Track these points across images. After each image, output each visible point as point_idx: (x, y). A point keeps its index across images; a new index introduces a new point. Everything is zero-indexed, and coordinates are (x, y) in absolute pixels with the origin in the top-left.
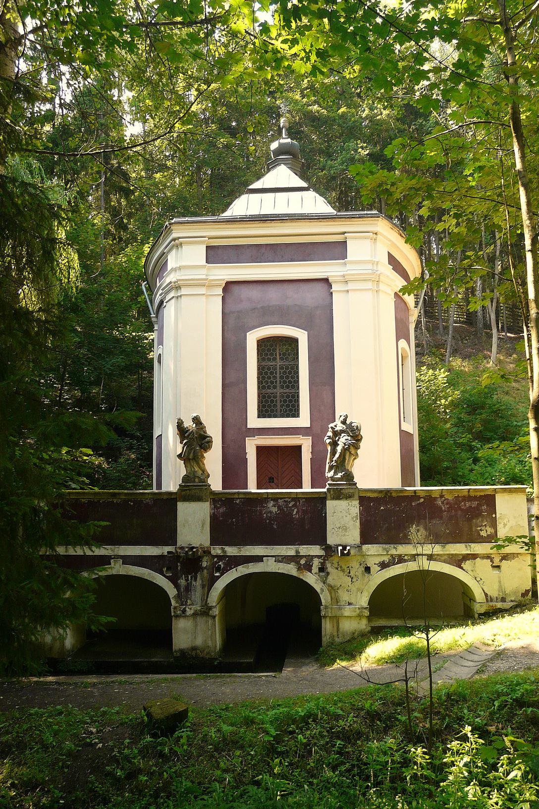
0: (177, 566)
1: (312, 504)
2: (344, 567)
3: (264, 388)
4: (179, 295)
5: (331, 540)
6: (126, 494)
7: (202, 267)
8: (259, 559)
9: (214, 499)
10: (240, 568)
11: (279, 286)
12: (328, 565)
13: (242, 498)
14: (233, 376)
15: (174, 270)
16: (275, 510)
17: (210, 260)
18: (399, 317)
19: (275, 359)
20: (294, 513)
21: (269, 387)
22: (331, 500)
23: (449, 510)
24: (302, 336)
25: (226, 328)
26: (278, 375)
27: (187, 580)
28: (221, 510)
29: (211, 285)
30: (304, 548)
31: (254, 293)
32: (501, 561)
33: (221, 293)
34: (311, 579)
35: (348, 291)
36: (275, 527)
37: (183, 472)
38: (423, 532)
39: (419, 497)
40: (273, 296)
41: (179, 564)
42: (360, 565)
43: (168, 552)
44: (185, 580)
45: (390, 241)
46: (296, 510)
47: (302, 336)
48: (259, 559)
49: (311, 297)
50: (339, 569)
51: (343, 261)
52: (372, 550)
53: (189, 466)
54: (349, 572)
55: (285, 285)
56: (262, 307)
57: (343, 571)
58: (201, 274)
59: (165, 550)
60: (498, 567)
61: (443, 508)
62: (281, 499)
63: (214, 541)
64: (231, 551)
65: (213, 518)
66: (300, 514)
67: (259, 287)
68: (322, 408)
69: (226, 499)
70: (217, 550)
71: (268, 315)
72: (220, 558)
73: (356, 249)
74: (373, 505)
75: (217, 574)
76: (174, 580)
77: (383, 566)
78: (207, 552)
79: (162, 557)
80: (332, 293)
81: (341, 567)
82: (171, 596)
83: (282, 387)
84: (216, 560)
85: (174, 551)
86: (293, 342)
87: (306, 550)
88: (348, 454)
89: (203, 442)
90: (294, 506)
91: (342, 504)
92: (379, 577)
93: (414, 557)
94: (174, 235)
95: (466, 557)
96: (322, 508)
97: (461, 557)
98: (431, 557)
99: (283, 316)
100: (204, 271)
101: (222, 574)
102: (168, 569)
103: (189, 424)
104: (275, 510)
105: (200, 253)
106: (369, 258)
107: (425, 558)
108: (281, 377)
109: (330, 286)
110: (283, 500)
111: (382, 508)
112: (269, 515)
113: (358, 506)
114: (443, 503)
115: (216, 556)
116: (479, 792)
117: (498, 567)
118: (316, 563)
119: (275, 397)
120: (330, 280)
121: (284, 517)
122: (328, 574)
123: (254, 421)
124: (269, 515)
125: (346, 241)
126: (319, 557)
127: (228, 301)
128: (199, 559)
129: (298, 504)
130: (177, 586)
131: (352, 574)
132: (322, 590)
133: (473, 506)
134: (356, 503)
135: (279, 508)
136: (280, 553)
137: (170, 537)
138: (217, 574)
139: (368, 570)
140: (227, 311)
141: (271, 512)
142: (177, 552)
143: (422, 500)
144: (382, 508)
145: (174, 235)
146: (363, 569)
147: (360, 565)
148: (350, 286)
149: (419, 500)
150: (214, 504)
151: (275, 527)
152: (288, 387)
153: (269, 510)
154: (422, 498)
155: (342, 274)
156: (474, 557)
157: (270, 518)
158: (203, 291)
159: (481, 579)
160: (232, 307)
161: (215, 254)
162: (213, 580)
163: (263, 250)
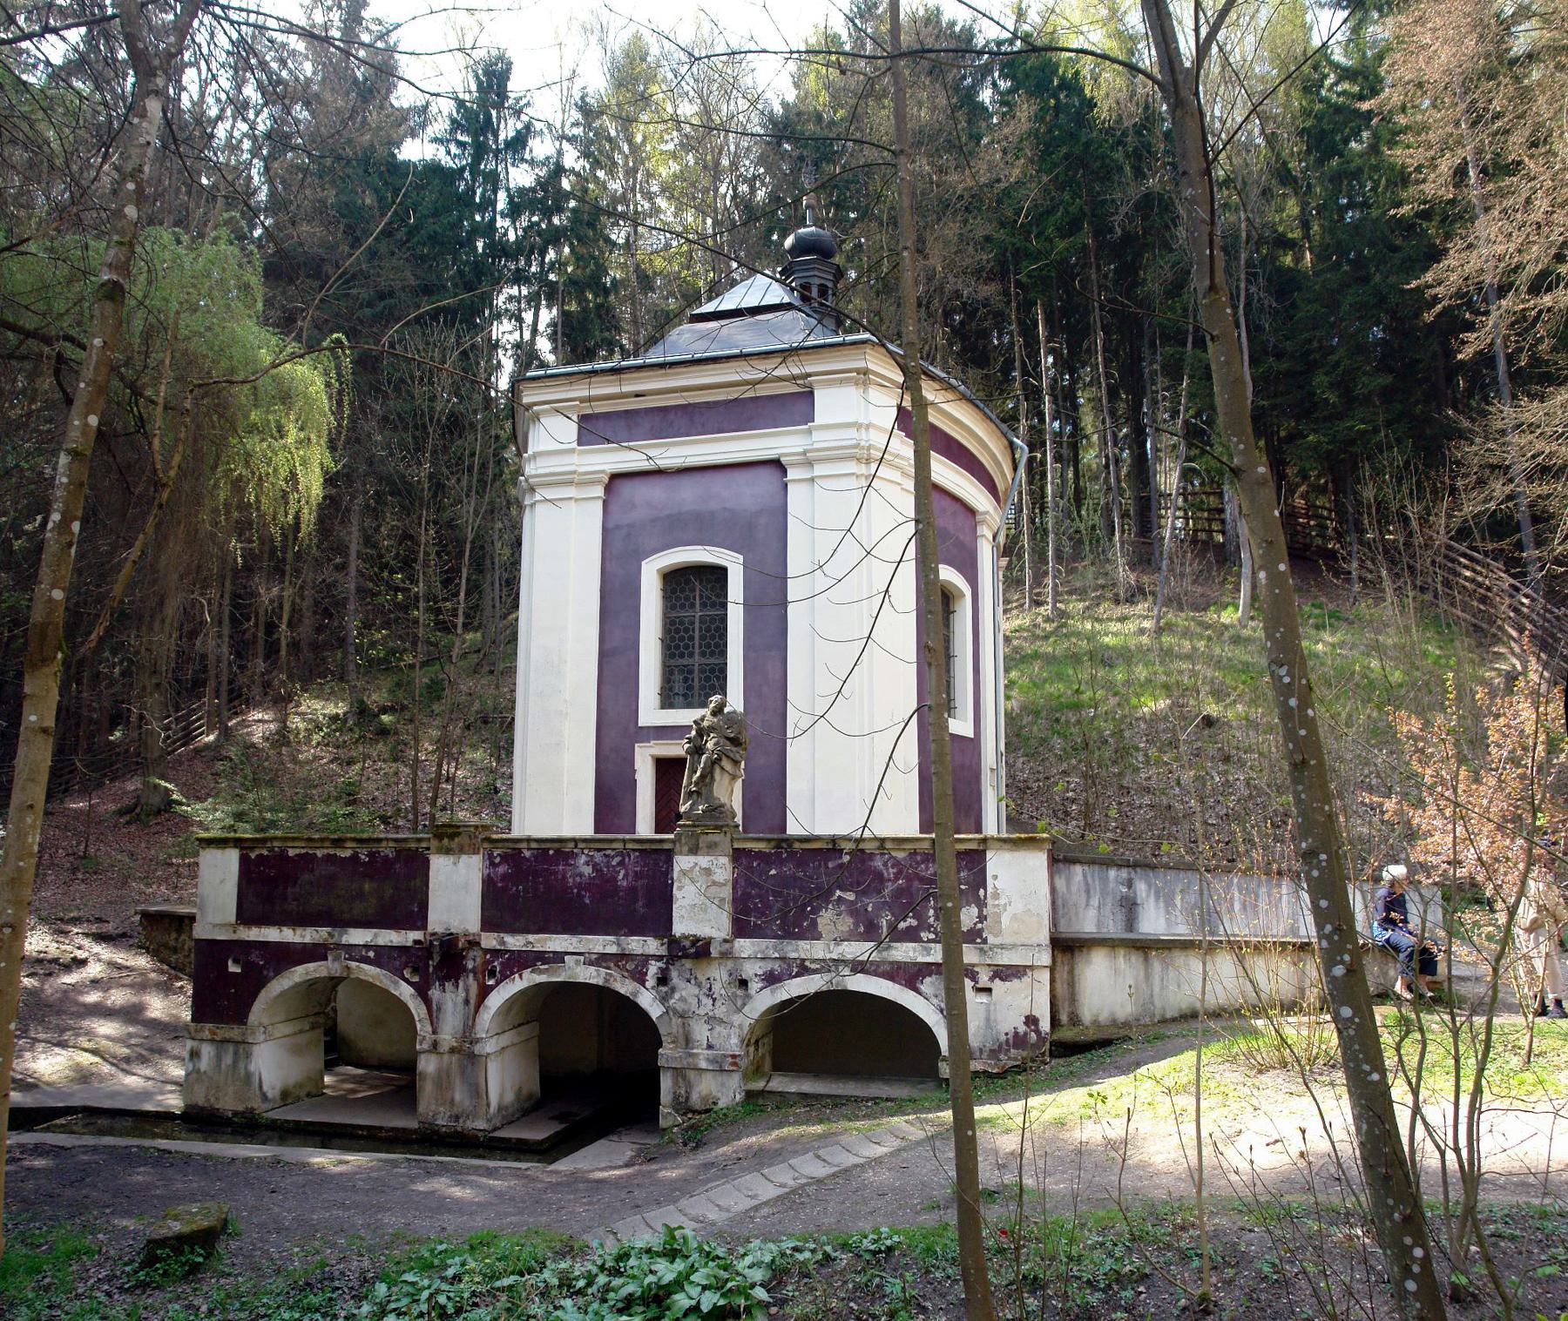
2: (702, 978)
5: (679, 928)
7: (572, 451)
8: (559, 957)
10: (526, 973)
11: (698, 477)
12: (674, 974)
16: (587, 870)
19: (693, 606)
26: (697, 634)
28: (501, 870)
29: (585, 481)
32: (992, 979)
34: (648, 1001)
35: (812, 480)
40: (688, 494)
43: (416, 942)
49: (750, 492)
56: (669, 516)
57: (699, 985)
59: (409, 937)
60: (989, 990)
63: (488, 924)
64: (515, 942)
65: (488, 884)
70: (489, 941)
71: (678, 529)
72: (496, 953)
73: (832, 404)
75: (491, 982)
77: (771, 979)
78: (474, 943)
79: (402, 949)
83: (691, 655)
86: (717, 575)
87: (640, 945)
90: (621, 863)
92: (764, 1000)
98: (859, 967)
99: (700, 528)
100: (575, 459)
101: (497, 984)
102: (415, 971)
104: (587, 870)
105: (567, 430)
108: (702, 638)
109: (784, 472)
111: (773, 872)
113: (729, 867)
114: (885, 864)
116: (1411, 907)
117: (989, 990)
118: (653, 969)
120: (783, 459)
121: (603, 884)
122: (673, 990)
123: (650, 712)
125: (811, 393)
126: (659, 958)
127: (613, 507)
135: (595, 867)
137: (418, 918)
138: (491, 982)
141: (581, 875)
148: (819, 470)
157: (580, 886)
158: (570, 492)
160: (617, 517)
161: (593, 428)
162: (485, 992)
163: (671, 417)
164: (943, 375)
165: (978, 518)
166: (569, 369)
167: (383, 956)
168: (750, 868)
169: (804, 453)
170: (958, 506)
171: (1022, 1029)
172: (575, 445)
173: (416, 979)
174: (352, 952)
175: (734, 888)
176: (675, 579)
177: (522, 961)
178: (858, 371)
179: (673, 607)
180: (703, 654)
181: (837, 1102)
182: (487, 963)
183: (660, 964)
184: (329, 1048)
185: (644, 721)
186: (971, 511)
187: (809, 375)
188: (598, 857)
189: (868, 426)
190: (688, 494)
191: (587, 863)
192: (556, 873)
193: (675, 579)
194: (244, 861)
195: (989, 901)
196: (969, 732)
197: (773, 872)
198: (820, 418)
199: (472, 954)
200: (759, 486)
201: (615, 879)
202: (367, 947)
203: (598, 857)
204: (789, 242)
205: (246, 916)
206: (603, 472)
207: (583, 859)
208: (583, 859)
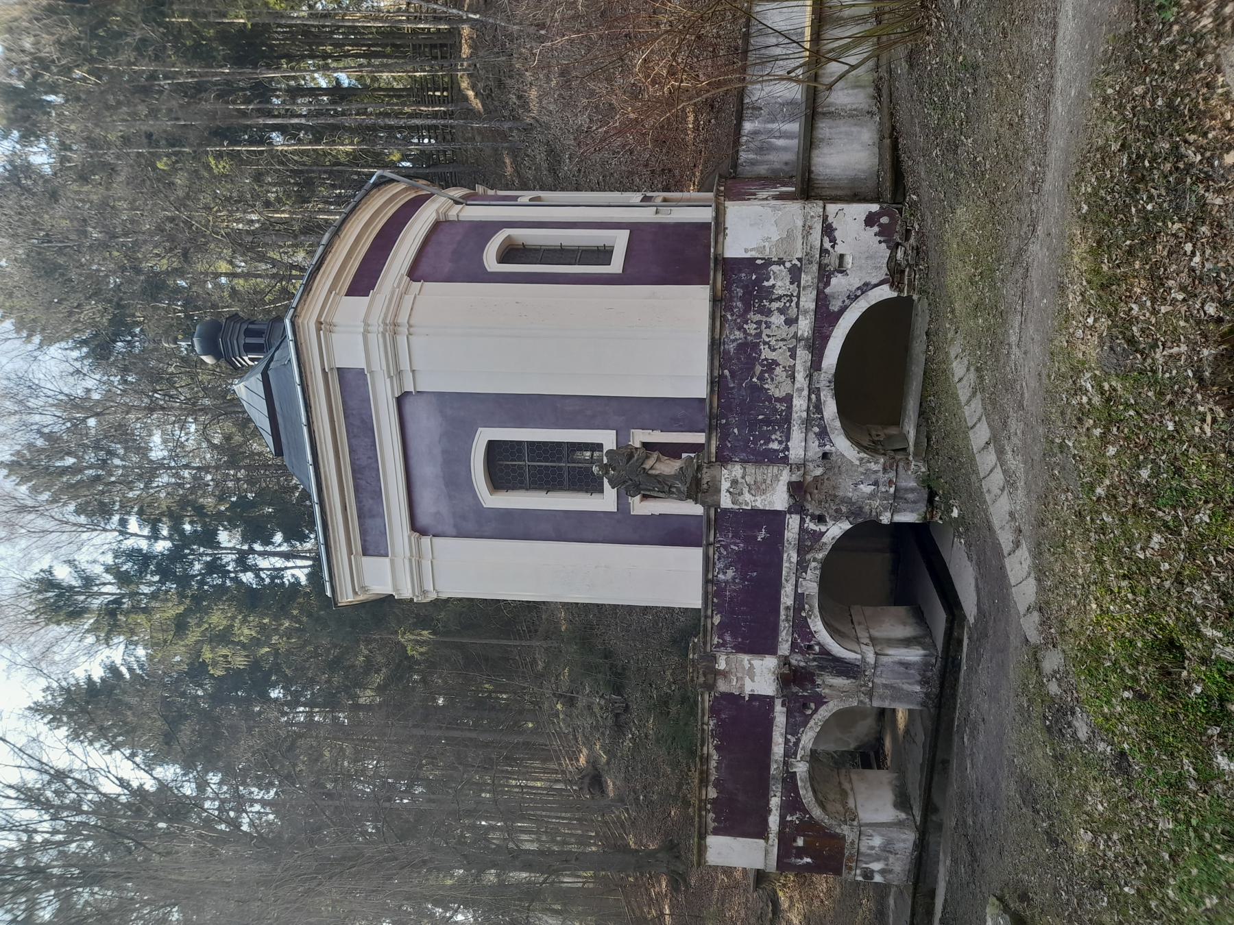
11: (413, 462)
17: (382, 552)
18: (447, 267)
28: (728, 638)
35: (413, 371)
40: (428, 471)
45: (330, 292)
46: (732, 547)
49: (425, 424)
56: (447, 485)
59: (778, 703)
63: (772, 651)
68: (589, 413)
70: (784, 648)
71: (457, 480)
72: (794, 645)
73: (349, 354)
78: (785, 661)
79: (789, 714)
86: (493, 448)
90: (725, 547)
92: (842, 445)
93: (814, 390)
100: (399, 561)
102: (805, 706)
104: (730, 573)
106: (360, 338)
111: (736, 431)
121: (742, 561)
126: (802, 521)
127: (440, 529)
138: (817, 648)
141: (734, 578)
146: (821, 455)
148: (405, 365)
155: (388, 381)
157: (743, 579)
158: (426, 564)
161: (373, 545)
163: (363, 483)
164: (321, 248)
165: (442, 218)
166: (319, 528)
167: (793, 728)
168: (734, 450)
169: (391, 377)
170: (430, 249)
171: (876, 229)
172: (387, 560)
173: (813, 705)
174: (790, 753)
175: (748, 462)
176: (498, 482)
177: (801, 627)
178: (319, 330)
179: (522, 482)
182: (802, 653)
183: (807, 520)
184: (866, 765)
186: (437, 226)
187: (324, 370)
188: (720, 565)
189: (366, 324)
191: (725, 573)
192: (731, 598)
193: (498, 482)
194: (716, 832)
195: (766, 254)
196: (625, 234)
197: (736, 431)
199: (794, 662)
201: (737, 553)
202: (787, 741)
203: (720, 565)
204: (208, 360)
207: (721, 576)
208: (721, 576)
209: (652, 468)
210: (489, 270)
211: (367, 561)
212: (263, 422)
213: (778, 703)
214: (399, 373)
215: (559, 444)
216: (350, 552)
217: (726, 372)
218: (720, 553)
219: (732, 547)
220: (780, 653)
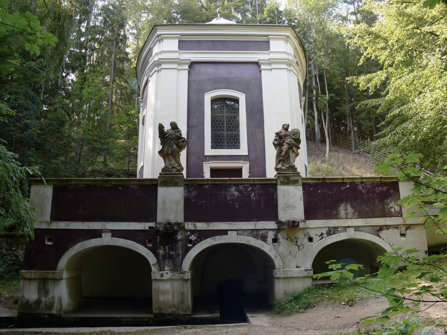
0: (157, 239)
1: (266, 189)
2: (293, 238)
3: (215, 130)
4: (160, 69)
6: (116, 180)
8: (224, 232)
9: (187, 185)
12: (280, 236)
13: (210, 184)
14: (194, 121)
15: (157, 54)
20: (252, 196)
21: (219, 130)
22: (281, 185)
23: (367, 193)
24: (242, 98)
25: (190, 90)
26: (225, 123)
27: (165, 250)
28: (193, 194)
29: (180, 62)
30: (260, 223)
31: (210, 69)
32: (406, 230)
33: (188, 68)
36: (237, 207)
37: (163, 165)
38: (350, 210)
39: (346, 184)
40: (222, 71)
41: (158, 237)
42: (305, 236)
43: (150, 227)
44: (163, 250)
46: (253, 194)
47: (242, 98)
48: (224, 232)
49: (249, 71)
50: (289, 239)
51: (268, 52)
52: (313, 223)
53: (167, 159)
54: (297, 242)
55: (231, 65)
56: (215, 78)
57: (292, 241)
58: (176, 56)
59: (152, 224)
61: (364, 192)
62: (242, 184)
63: (187, 218)
64: (201, 226)
65: (187, 201)
66: (257, 196)
67: (213, 66)
69: (198, 185)
70: (189, 226)
73: (275, 45)
74: (313, 189)
75: (190, 245)
76: (154, 251)
80: (261, 71)
81: (290, 238)
82: (151, 263)
84: (189, 233)
85: (154, 226)
86: (236, 101)
88: (291, 151)
89: (180, 141)
90: (252, 190)
91: (290, 189)
93: (345, 228)
94: (158, 33)
95: (381, 228)
96: (274, 192)
97: (379, 228)
101: (194, 246)
103: (167, 128)
104: (236, 193)
105: (173, 44)
106: (284, 51)
107: (353, 229)
108: (227, 124)
109: (260, 67)
110: (243, 186)
111: (319, 192)
112: (232, 197)
113: (302, 189)
114: (363, 188)
115: (188, 231)
119: (224, 137)
123: (209, 151)
124: (232, 197)
125: (269, 41)
128: (175, 232)
129: (255, 188)
130: (156, 255)
131: (299, 243)
132: (276, 257)
133: (384, 190)
134: (301, 188)
135: (240, 192)
136: (241, 227)
138: (190, 245)
139: (311, 240)
140: (192, 80)
141: (233, 195)
142: (157, 227)
143: (348, 186)
144: (319, 192)
145: (158, 33)
147: (305, 236)
148: (273, 66)
149: (346, 186)
150: (187, 189)
151: (237, 207)
152: (231, 130)
153: (231, 193)
154: (348, 184)
156: (388, 227)
158: (175, 66)
159: (393, 244)
163: (216, 44)
169: (268, 60)
172: (177, 49)
173: (150, 245)
180: (223, 130)
181: (242, 326)
185: (206, 154)
190: (222, 71)
198: (271, 49)
200: (249, 71)
205: (55, 217)
206: (190, 60)
209: (293, 151)
210: (205, 94)
211: (176, 42)
212: (207, 23)
213: (152, 224)
214: (270, 64)
215: (212, 133)
216: (182, 35)
217: (348, 186)
218: (248, 187)
219: (253, 194)
220: (186, 224)
